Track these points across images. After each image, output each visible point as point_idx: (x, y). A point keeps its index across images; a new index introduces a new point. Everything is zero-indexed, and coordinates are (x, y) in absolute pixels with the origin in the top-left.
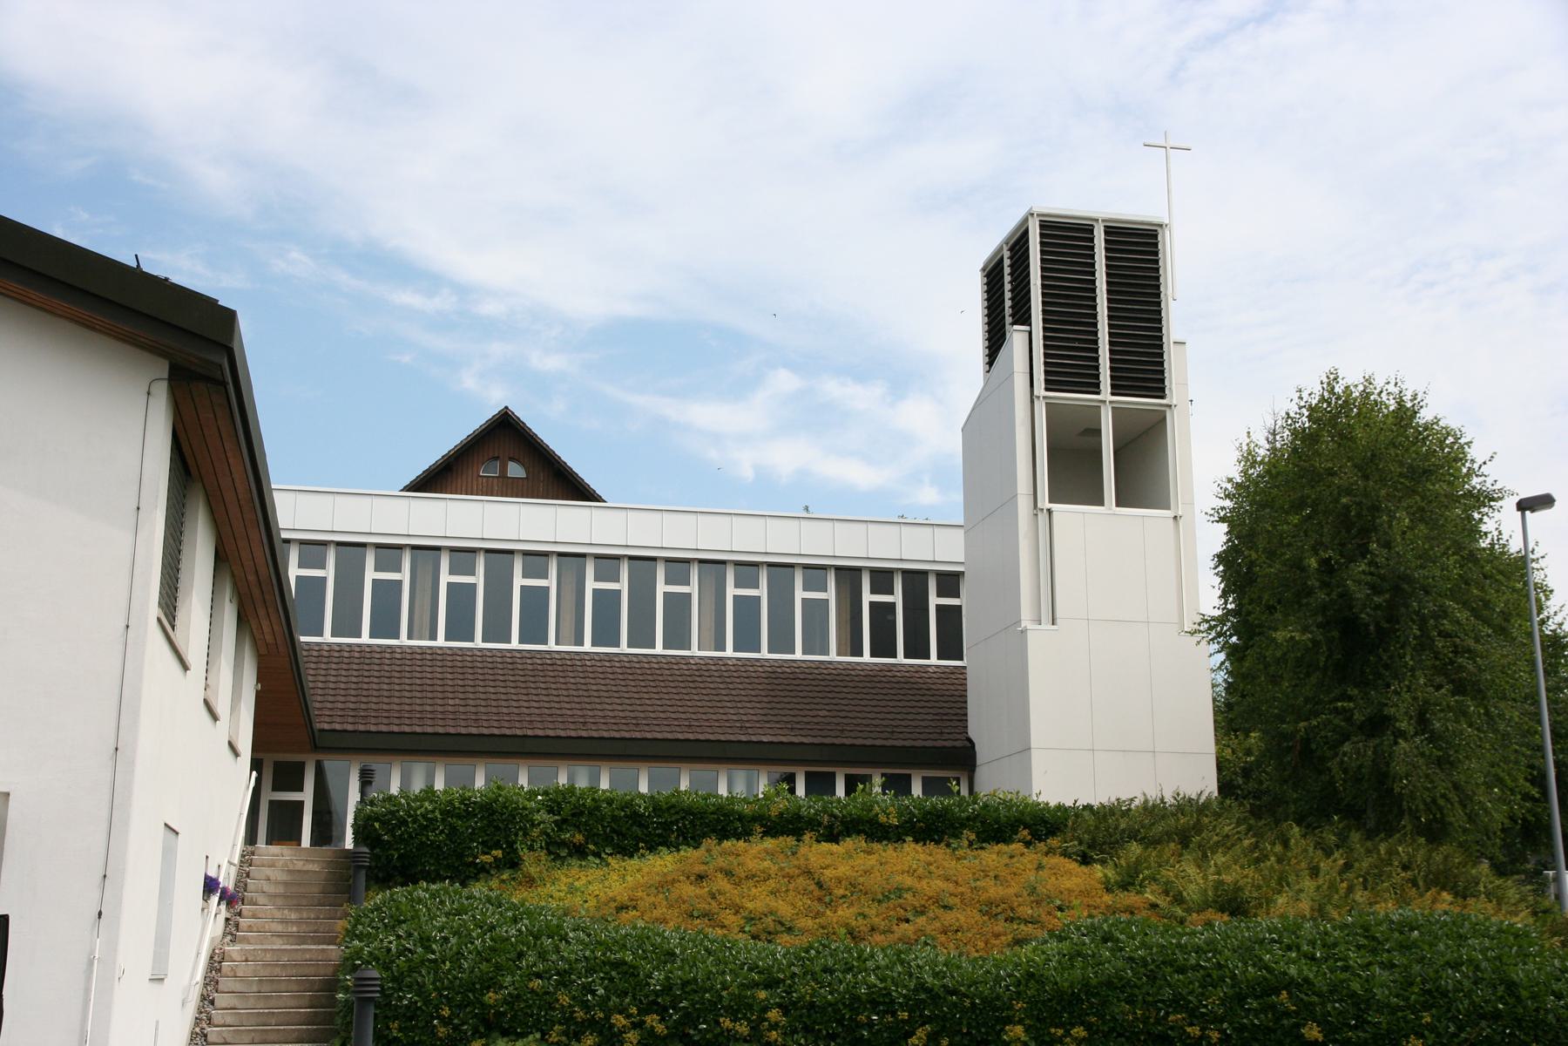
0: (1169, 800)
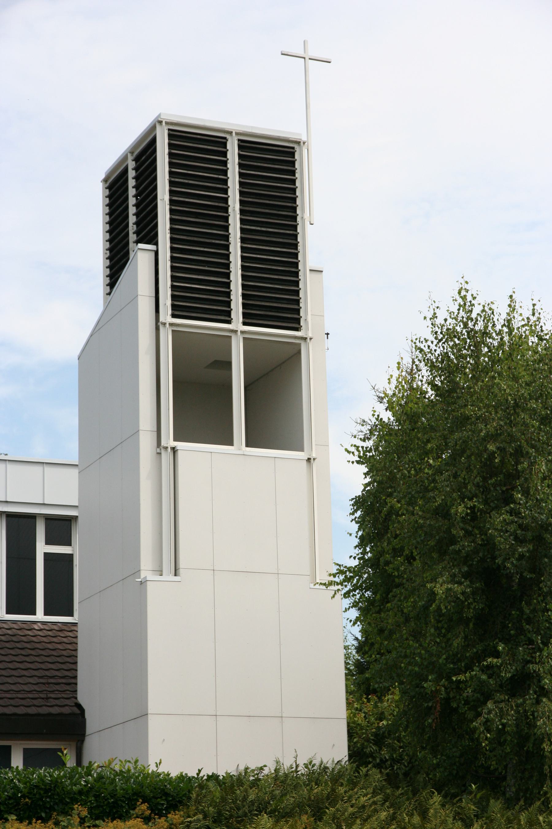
0: (302, 770)
